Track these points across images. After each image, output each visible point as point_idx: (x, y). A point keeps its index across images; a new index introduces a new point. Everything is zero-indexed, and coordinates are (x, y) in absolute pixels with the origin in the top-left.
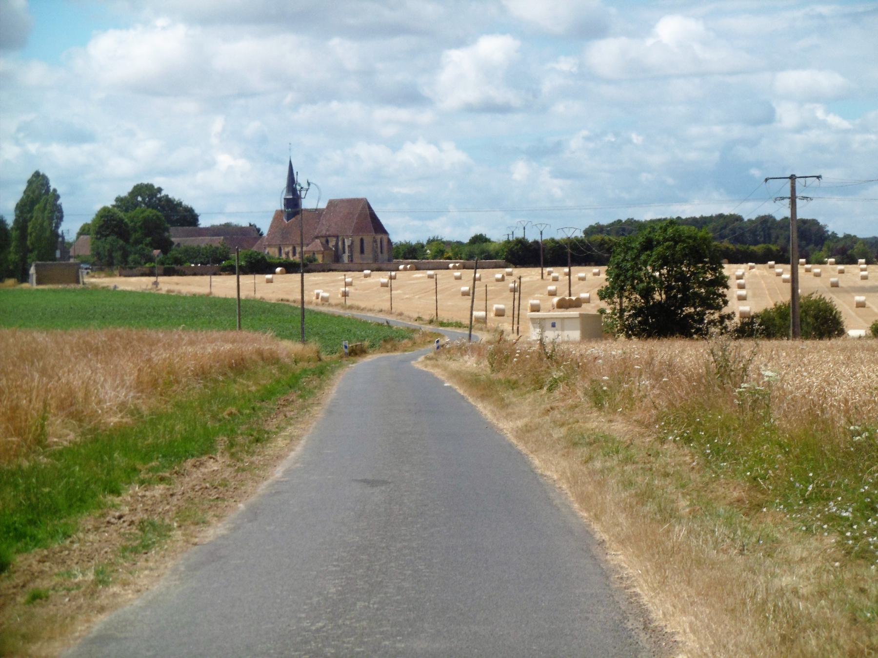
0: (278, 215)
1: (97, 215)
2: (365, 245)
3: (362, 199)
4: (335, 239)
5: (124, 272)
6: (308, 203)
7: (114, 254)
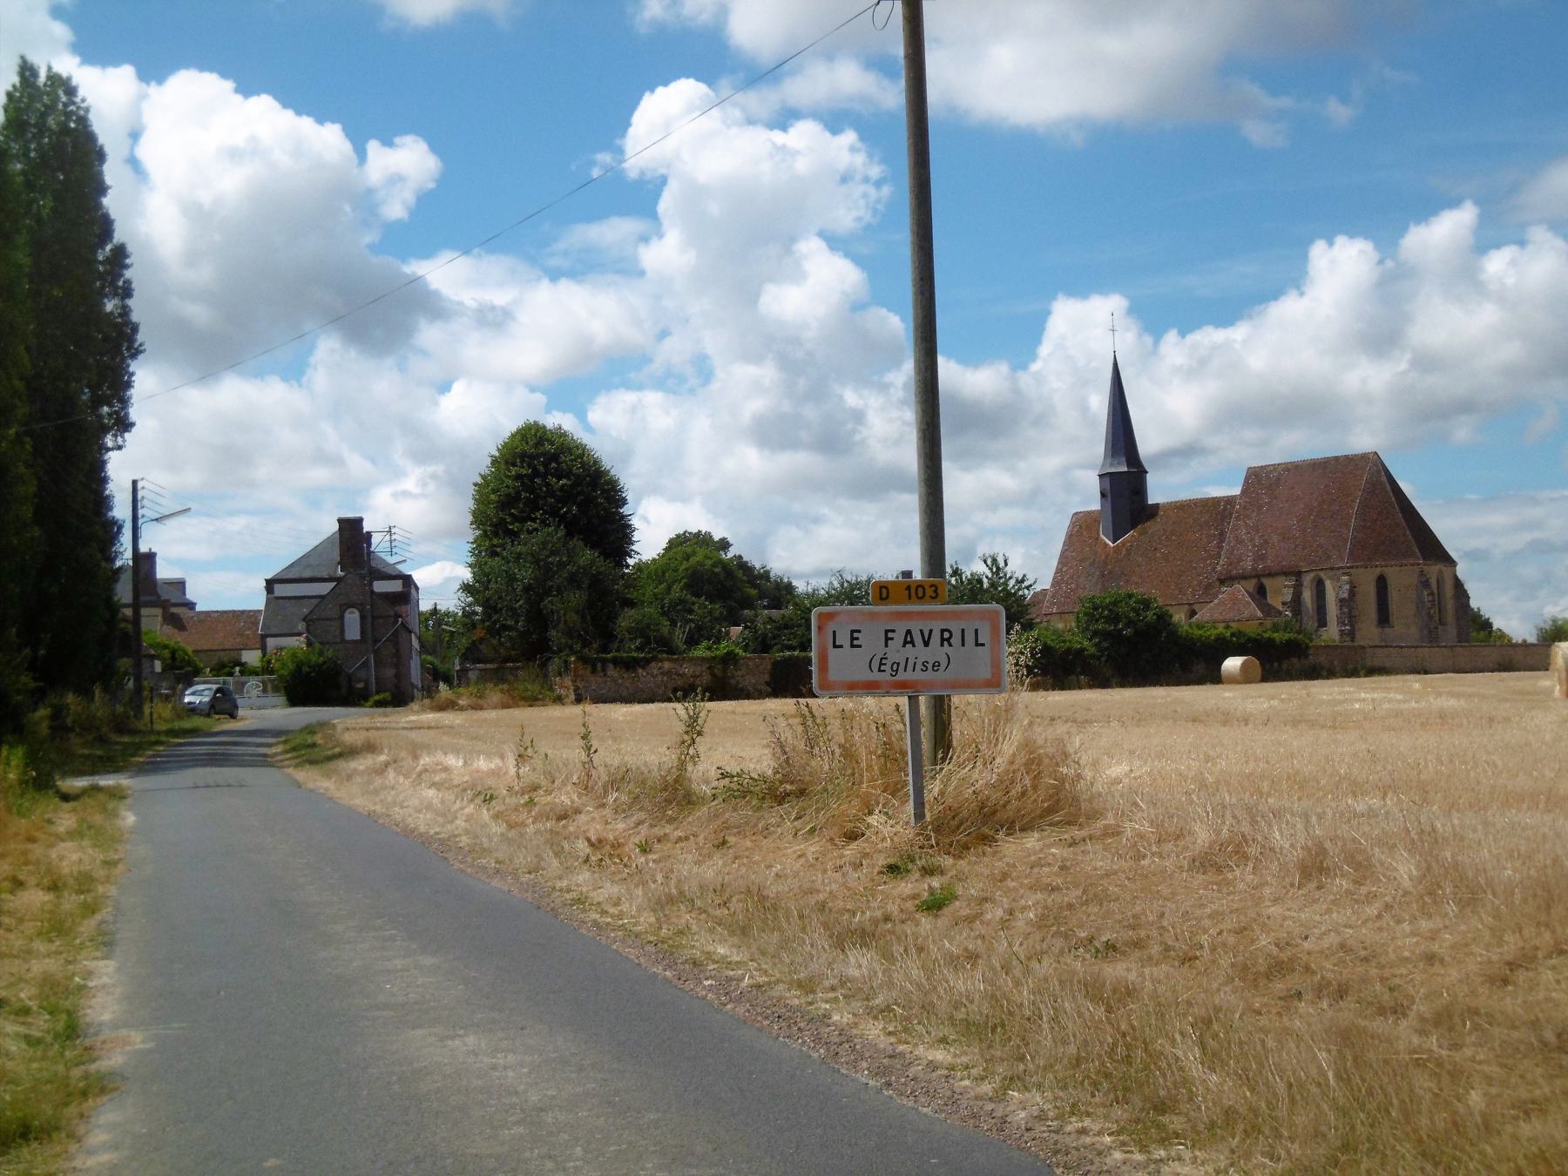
0: (1082, 527)
1: (495, 462)
2: (1394, 596)
3: (1364, 457)
4: (1290, 582)
5: (595, 682)
6: (1161, 489)
7: (550, 603)
